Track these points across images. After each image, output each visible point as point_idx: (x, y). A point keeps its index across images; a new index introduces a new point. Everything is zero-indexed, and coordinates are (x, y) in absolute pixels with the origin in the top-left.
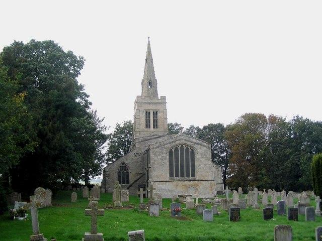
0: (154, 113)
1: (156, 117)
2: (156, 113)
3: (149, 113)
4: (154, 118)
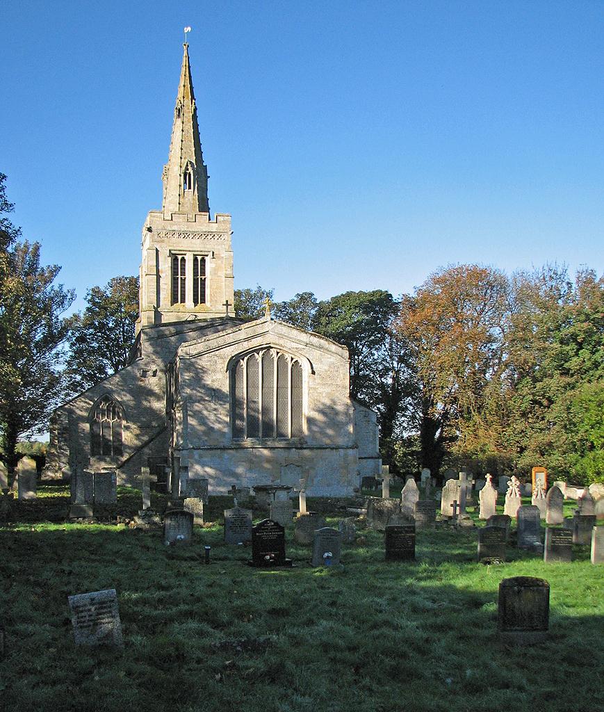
0: (195, 260)
1: (203, 273)
2: (203, 261)
3: (183, 260)
4: (195, 273)
